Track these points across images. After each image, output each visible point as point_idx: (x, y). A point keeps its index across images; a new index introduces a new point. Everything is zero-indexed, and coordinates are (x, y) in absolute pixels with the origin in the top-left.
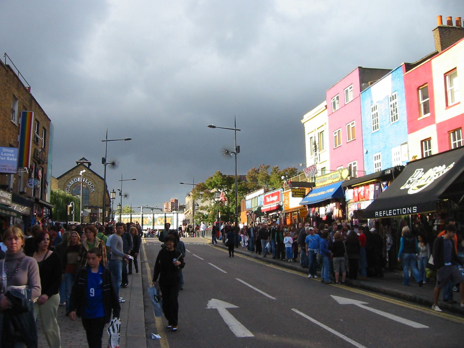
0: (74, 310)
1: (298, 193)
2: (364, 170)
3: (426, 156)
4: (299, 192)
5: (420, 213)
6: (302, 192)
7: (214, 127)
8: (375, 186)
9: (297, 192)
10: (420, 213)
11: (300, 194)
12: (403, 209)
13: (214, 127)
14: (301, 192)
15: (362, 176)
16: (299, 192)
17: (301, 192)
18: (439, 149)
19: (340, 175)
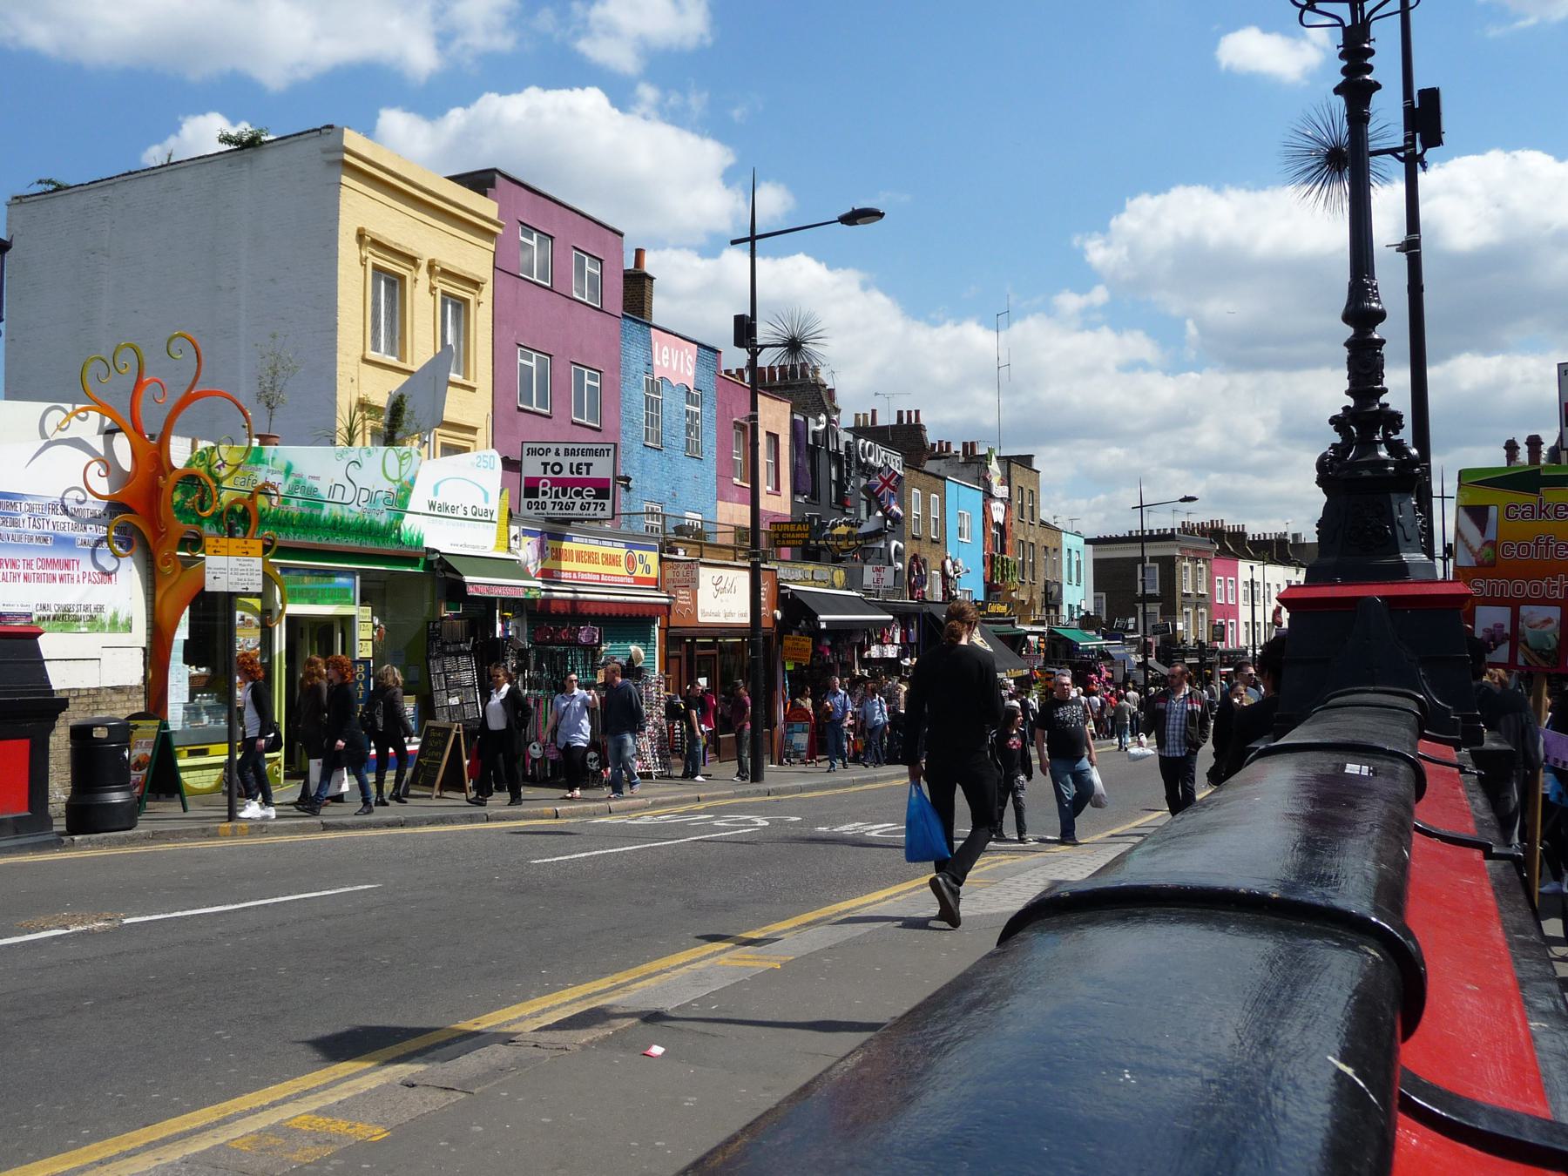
0: (1081, 253)
1: (789, 536)
2: (1397, 12)
3: (411, 751)
4: (791, 533)
5: (1538, 839)
6: (800, 532)
7: (852, 218)
8: (1275, 550)
9: (787, 532)
10: (1538, 839)
11: (793, 536)
12: (1230, 621)
13: (852, 218)
14: (795, 532)
15: (1406, 263)
16: (791, 533)
17: (795, 532)
18: (747, 504)
19: (829, 578)
